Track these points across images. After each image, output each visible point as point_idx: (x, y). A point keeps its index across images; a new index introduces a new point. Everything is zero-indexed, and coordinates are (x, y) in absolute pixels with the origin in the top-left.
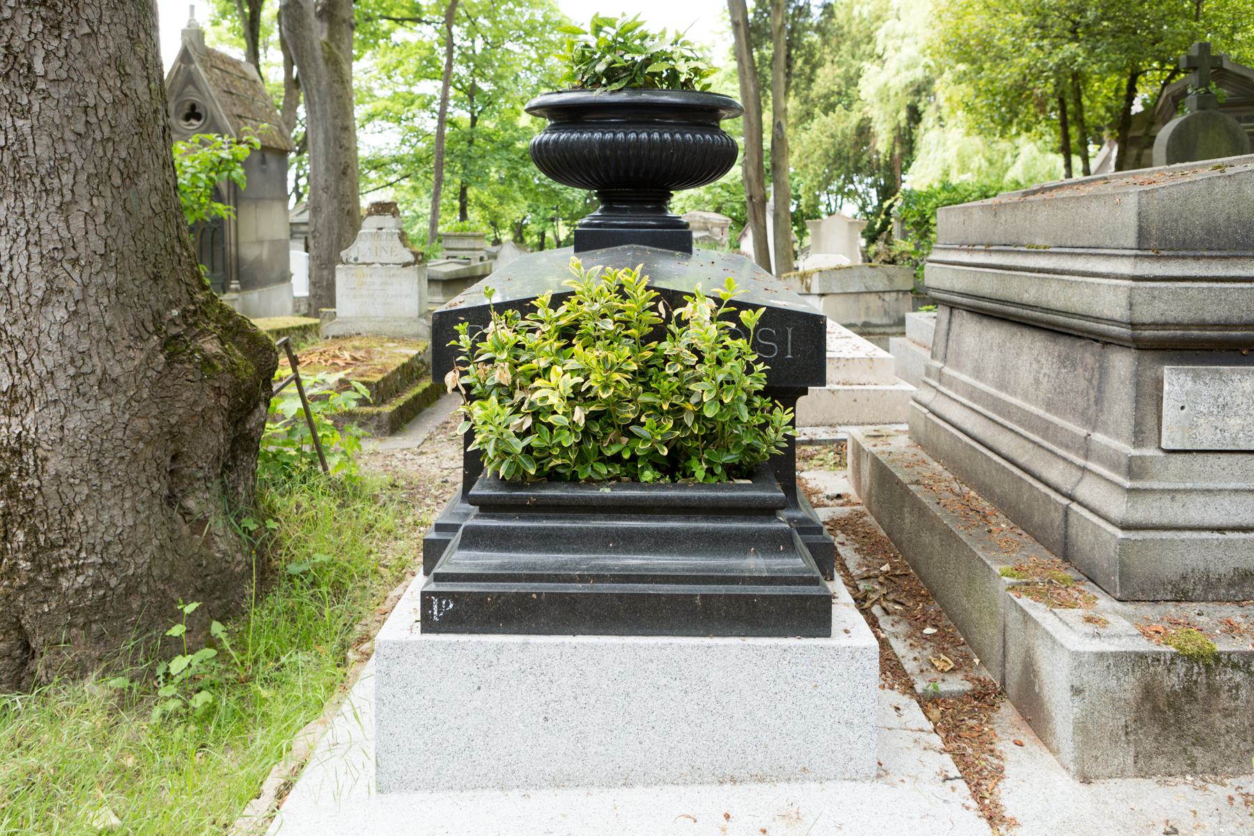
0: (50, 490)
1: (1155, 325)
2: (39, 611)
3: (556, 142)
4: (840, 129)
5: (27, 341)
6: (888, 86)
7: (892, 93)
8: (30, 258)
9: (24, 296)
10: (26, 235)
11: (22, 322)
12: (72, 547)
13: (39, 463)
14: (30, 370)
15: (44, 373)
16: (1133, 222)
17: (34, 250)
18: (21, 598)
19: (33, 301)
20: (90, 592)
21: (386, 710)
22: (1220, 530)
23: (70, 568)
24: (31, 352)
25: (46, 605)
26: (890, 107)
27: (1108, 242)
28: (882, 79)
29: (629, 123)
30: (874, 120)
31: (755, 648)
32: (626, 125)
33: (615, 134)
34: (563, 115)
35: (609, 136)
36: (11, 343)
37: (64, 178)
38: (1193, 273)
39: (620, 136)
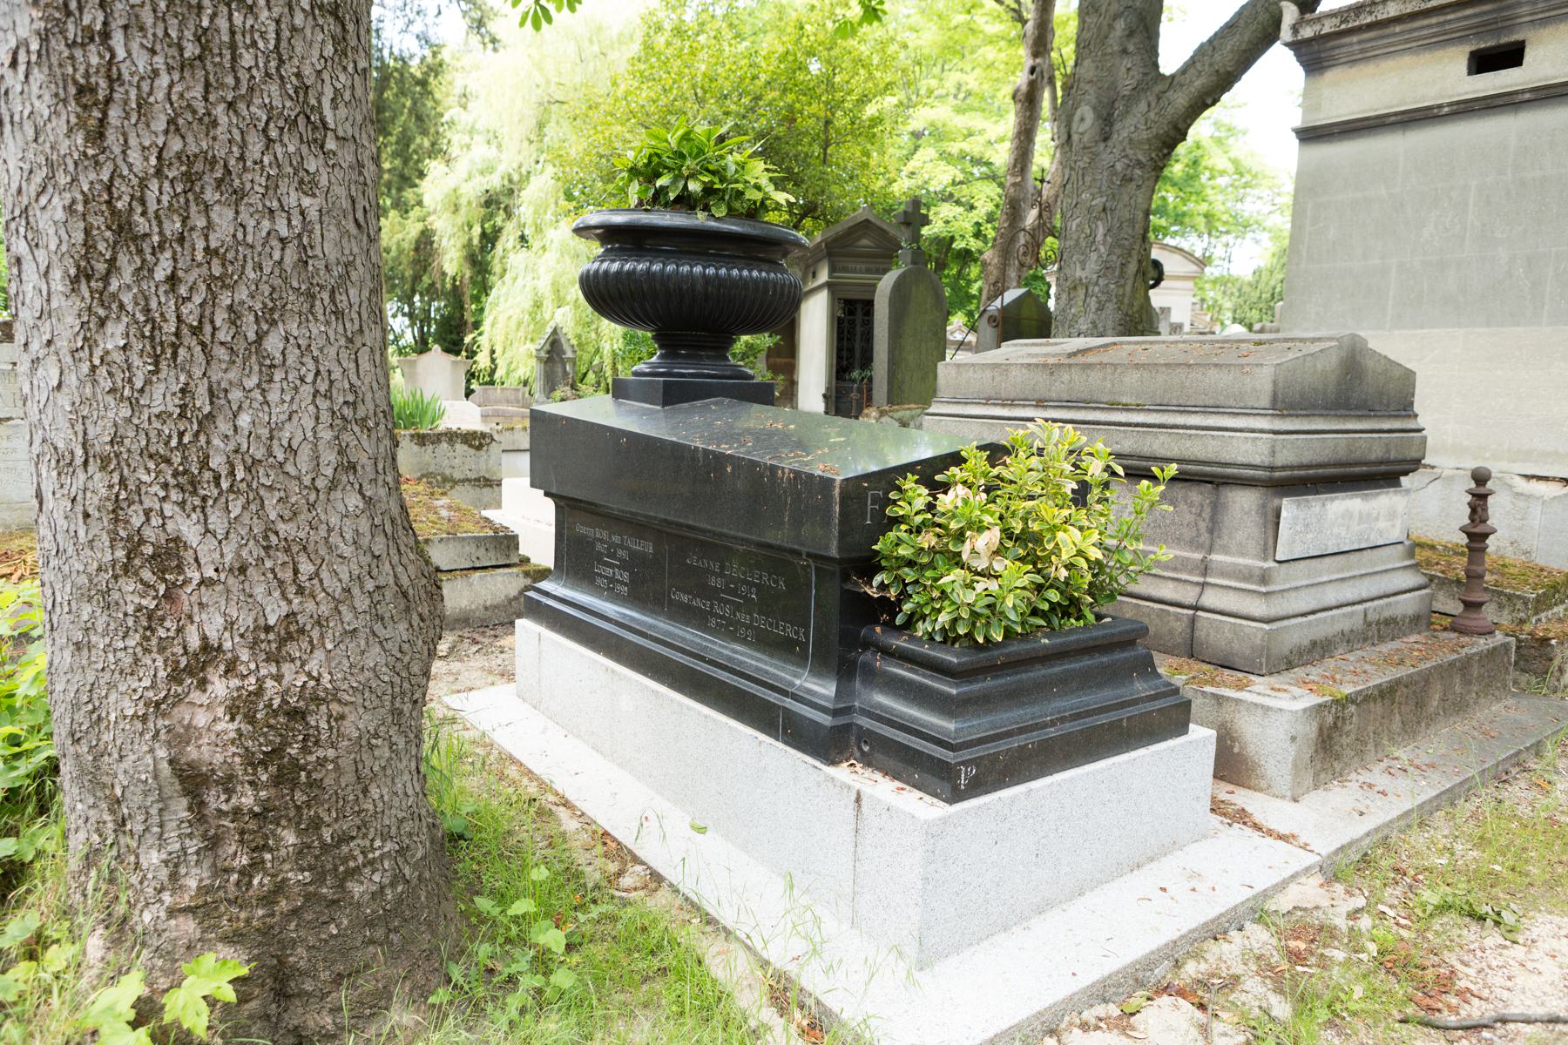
0: (346, 762)
1: (1283, 468)
2: (324, 936)
3: (619, 273)
4: (395, 240)
5: (312, 544)
6: (459, 192)
7: (463, 201)
8: (317, 418)
9: (309, 477)
10: (314, 382)
11: (304, 517)
12: (365, 836)
13: (333, 724)
14: (318, 588)
15: (339, 590)
16: (1268, 387)
17: (324, 404)
18: (292, 926)
19: (321, 483)
20: (388, 891)
21: (930, 887)
22: (1304, 615)
23: (364, 866)
24: (319, 562)
25: (333, 926)
26: (461, 218)
27: (1233, 403)
28: (451, 182)
29: (681, 252)
30: (438, 233)
31: (1158, 753)
32: (678, 255)
33: (691, 267)
34: (617, 237)
35: (711, 271)
36: (287, 550)
37: (352, 292)
38: (1291, 428)
39: (723, 271)
